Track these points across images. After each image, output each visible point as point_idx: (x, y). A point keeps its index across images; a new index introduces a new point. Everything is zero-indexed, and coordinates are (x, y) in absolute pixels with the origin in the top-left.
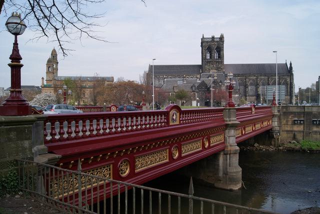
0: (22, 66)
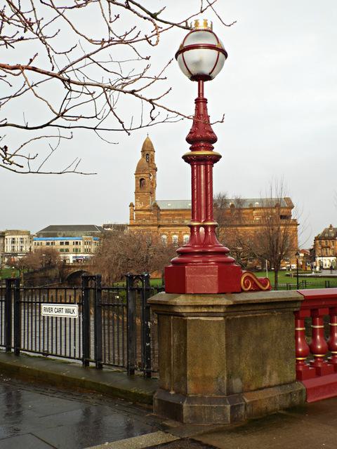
0: (217, 158)
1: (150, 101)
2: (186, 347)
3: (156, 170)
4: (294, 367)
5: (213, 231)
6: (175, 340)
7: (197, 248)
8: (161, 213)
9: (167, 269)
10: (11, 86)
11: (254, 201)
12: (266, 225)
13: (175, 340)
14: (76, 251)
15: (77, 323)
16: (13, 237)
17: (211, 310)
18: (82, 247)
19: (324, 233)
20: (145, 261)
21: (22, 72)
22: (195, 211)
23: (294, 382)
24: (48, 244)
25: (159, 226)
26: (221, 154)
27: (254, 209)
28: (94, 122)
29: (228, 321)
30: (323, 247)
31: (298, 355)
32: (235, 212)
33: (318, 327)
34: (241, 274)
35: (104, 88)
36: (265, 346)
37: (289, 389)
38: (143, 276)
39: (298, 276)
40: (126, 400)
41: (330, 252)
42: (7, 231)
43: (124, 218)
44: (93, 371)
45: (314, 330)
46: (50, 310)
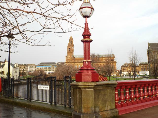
0: (91, 41)
1: (71, 22)
2: (82, 98)
3: (74, 46)
4: (115, 104)
5: (90, 63)
6: (78, 96)
7: (85, 68)
8: (75, 59)
9: (76, 74)
10: (18, 7)
11: (103, 55)
12: (107, 62)
13: (78, 96)
14: (49, 70)
15: (49, 91)
16: (30, 66)
17: (89, 87)
18: (51, 69)
19: (124, 65)
20: (70, 73)
21: (32, 14)
22: (85, 57)
23: (115, 109)
24: (41, 68)
25: (75, 63)
26: (92, 39)
27: (103, 58)
28: (54, 30)
29: (95, 90)
30: (124, 69)
31: (116, 101)
32: (97, 59)
33: (122, 92)
34: (99, 76)
35: (57, 18)
36: (106, 98)
37: (113, 111)
38: (69, 76)
39: (116, 78)
40: (64, 115)
41: (126, 71)
42: (28, 64)
43: (64, 60)
44: (54, 106)
45: (121, 93)
46: (40, 87)
